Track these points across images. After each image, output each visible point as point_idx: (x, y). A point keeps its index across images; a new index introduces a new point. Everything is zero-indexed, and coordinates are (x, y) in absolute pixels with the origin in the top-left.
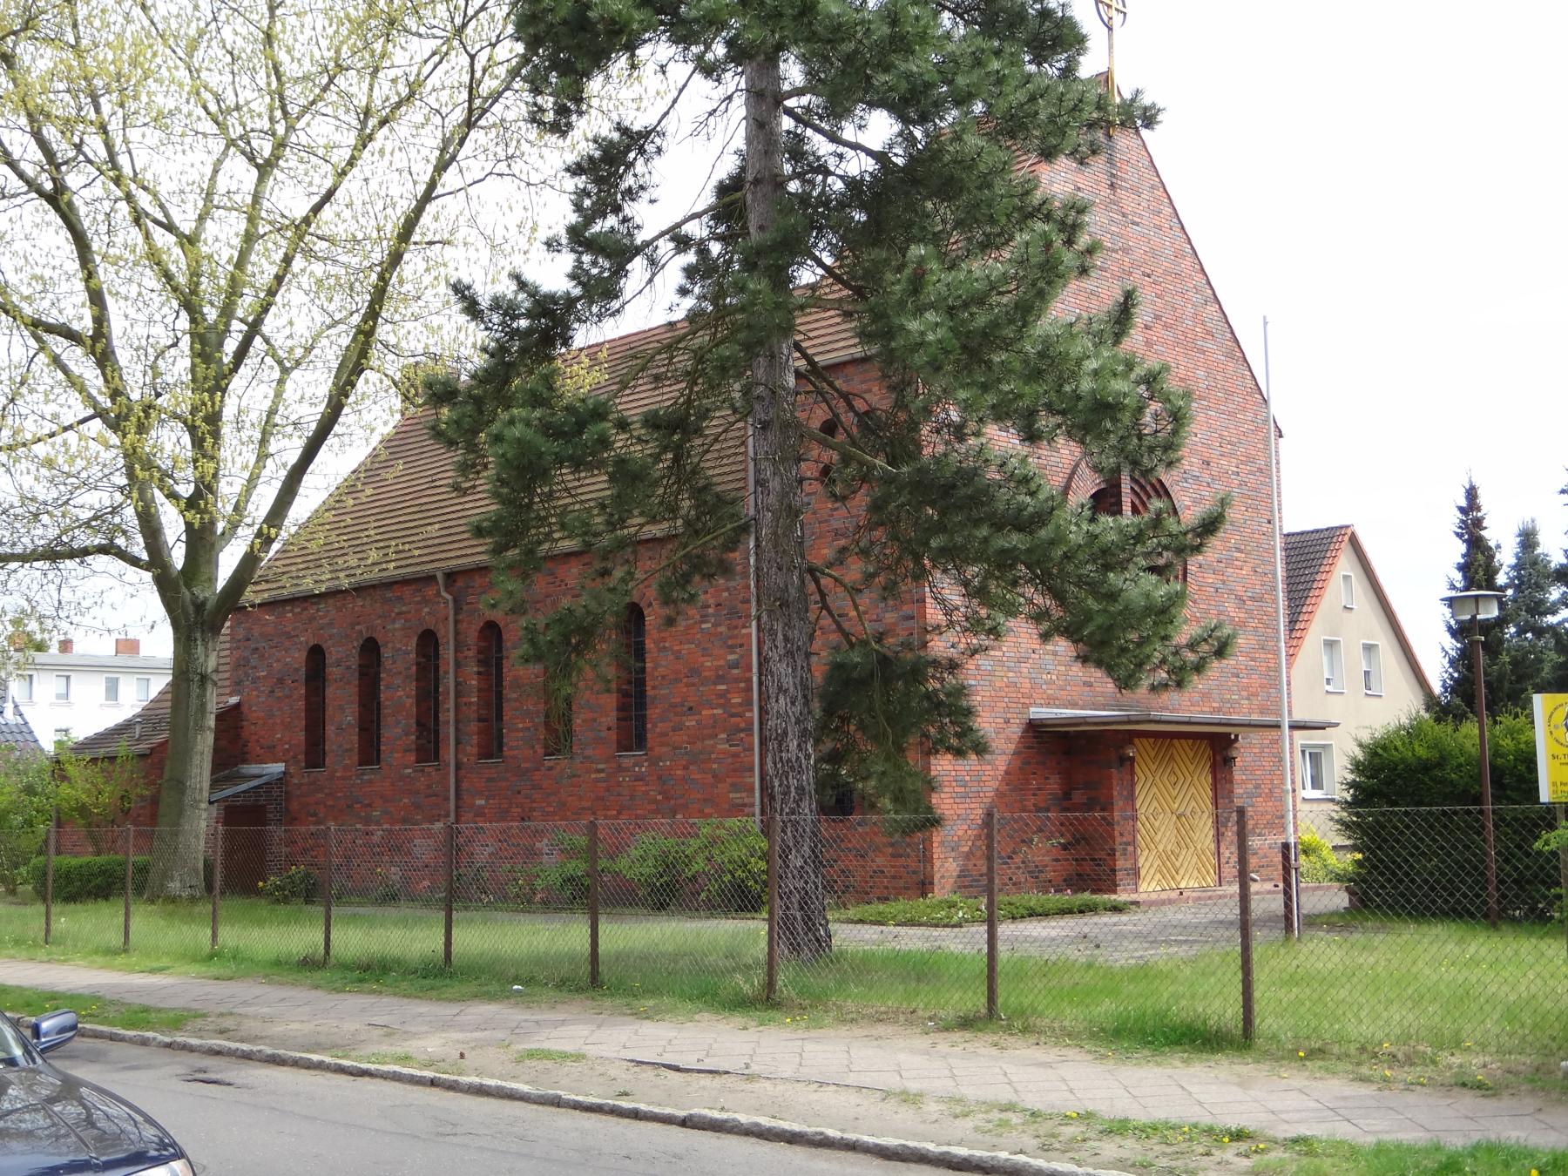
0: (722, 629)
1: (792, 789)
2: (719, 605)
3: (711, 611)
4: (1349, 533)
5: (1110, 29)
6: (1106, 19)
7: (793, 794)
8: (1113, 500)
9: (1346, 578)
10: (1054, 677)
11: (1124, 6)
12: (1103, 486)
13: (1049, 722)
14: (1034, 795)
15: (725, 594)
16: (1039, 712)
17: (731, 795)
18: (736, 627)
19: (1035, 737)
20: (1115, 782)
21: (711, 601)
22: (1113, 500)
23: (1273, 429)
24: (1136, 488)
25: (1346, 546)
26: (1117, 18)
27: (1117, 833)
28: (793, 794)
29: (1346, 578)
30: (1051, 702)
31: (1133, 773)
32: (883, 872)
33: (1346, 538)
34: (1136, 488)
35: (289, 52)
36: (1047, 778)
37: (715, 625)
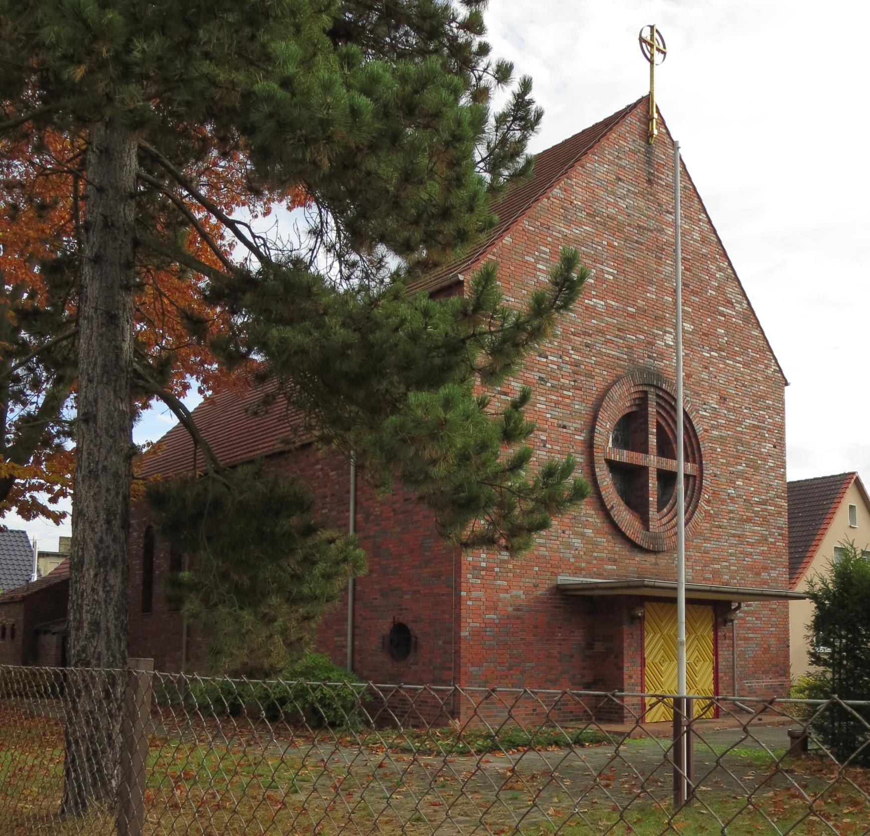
0: (334, 513)
1: (86, 625)
2: (333, 495)
3: (328, 500)
4: (855, 478)
5: (651, 62)
6: (649, 55)
7: (86, 630)
8: (642, 420)
9: (852, 508)
10: (582, 553)
11: (665, 47)
12: (634, 409)
13: (572, 587)
14: (559, 644)
15: (337, 487)
16: (565, 579)
17: (336, 639)
18: (342, 512)
19: (561, 599)
20: (625, 636)
21: (329, 493)
22: (642, 420)
23: (680, 169)
24: (663, 413)
25: (851, 486)
26: (658, 57)
27: (626, 677)
28: (86, 630)
29: (852, 508)
30: (577, 571)
31: (642, 630)
32: (426, 702)
33: (853, 481)
34: (663, 413)
35: (396, 330)
36: (573, 632)
37: (330, 511)
